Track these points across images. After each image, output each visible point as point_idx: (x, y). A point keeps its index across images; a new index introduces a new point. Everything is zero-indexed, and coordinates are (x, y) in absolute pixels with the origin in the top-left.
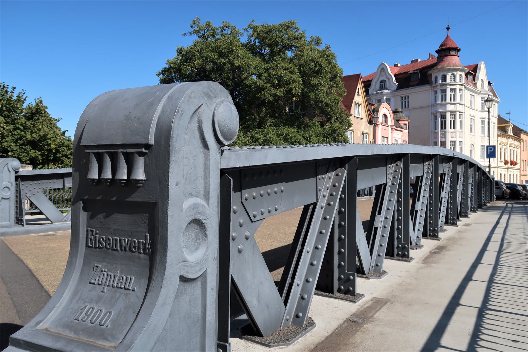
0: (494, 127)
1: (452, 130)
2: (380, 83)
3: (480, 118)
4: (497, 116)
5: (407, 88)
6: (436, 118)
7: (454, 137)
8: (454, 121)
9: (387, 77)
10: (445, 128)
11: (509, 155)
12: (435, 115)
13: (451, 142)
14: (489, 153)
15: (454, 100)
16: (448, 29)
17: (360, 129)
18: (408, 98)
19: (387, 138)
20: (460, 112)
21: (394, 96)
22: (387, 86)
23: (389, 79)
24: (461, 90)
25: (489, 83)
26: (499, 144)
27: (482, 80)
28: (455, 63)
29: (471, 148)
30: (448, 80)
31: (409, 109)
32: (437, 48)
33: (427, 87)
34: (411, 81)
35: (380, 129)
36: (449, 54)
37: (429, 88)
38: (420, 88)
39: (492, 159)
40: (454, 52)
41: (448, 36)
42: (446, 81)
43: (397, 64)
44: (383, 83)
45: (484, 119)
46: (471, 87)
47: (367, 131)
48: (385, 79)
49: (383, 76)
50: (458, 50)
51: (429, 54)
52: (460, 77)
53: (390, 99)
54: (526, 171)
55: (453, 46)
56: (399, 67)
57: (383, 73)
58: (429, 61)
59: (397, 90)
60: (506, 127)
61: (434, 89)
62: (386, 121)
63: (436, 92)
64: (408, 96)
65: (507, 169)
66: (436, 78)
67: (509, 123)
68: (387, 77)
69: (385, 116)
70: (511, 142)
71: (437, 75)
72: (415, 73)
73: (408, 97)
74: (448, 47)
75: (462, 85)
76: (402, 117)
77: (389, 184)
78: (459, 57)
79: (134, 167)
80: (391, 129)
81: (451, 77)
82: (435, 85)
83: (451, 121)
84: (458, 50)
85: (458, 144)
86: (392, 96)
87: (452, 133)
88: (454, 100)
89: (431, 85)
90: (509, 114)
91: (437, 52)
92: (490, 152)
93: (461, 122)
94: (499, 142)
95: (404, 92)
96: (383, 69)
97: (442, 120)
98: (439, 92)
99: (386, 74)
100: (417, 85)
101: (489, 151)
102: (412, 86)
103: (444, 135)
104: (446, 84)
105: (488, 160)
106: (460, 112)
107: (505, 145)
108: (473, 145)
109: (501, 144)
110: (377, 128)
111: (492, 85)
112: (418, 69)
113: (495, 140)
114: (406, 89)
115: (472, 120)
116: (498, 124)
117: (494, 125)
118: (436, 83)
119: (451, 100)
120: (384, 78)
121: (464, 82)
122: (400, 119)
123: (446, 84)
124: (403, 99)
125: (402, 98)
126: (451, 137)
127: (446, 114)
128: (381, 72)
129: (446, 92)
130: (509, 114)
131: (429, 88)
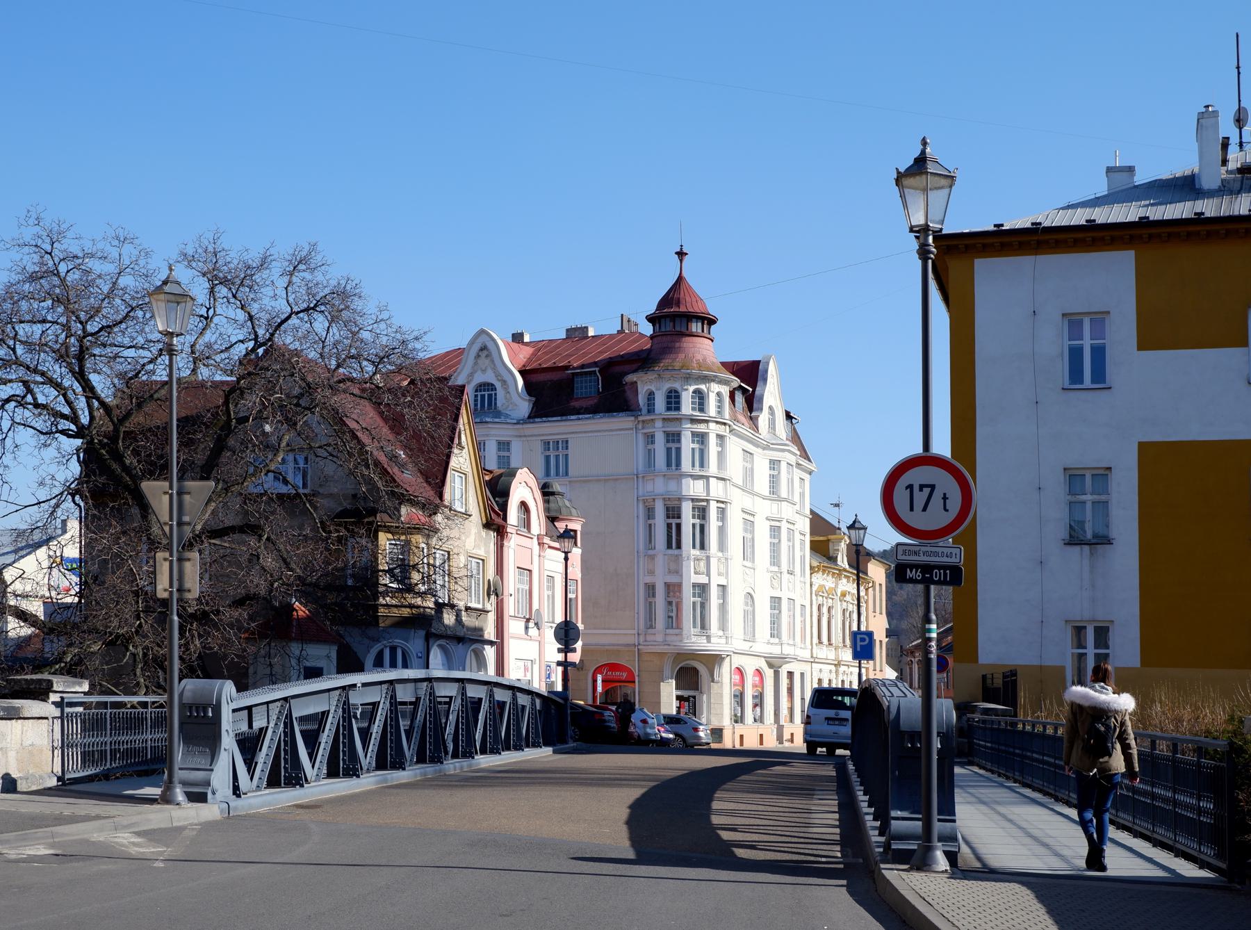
0: (803, 541)
1: (696, 552)
2: (476, 391)
3: (767, 519)
4: (808, 512)
5: (564, 418)
6: (650, 513)
7: (703, 574)
8: (702, 527)
9: (498, 376)
10: (679, 546)
11: (840, 625)
12: (647, 504)
13: (694, 585)
14: (859, 649)
15: (702, 465)
16: (681, 254)
17: (464, 546)
18: (567, 448)
19: (530, 571)
20: (718, 501)
21: (520, 436)
22: (499, 404)
23: (504, 382)
24: (720, 437)
25: (789, 416)
26: (814, 592)
27: (771, 408)
28: (704, 360)
29: (746, 604)
30: (687, 407)
31: (570, 482)
32: (652, 308)
33: (621, 422)
34: (575, 397)
35: (513, 543)
36: (687, 333)
37: (630, 425)
38: (603, 420)
39: (864, 662)
40: (700, 324)
41: (680, 279)
42: (678, 409)
43: (521, 335)
44: (486, 393)
45: (779, 521)
46: (744, 429)
47: (481, 552)
48: (494, 381)
49: (484, 371)
50: (712, 322)
51: (622, 315)
52: (719, 407)
53: (508, 443)
54: (881, 671)
55: (697, 309)
56: (527, 344)
57: (483, 362)
58: (621, 341)
59: (531, 420)
60: (831, 545)
61: (643, 428)
62: (527, 524)
63: (650, 439)
64: (567, 442)
65: (835, 665)
66: (651, 396)
67: (838, 531)
68: (498, 376)
69: (524, 506)
70: (845, 588)
71: (654, 390)
72: (584, 372)
73: (565, 445)
74: (683, 309)
75: (725, 424)
76: (564, 510)
77: (332, 711)
78: (712, 341)
79: (1100, 703)
80: (539, 544)
81: (692, 397)
82: (648, 418)
83: (694, 525)
84: (712, 322)
85: (714, 592)
86: (517, 436)
87: (697, 559)
88: (702, 465)
89: (636, 417)
90: (837, 505)
91: (651, 319)
92: (861, 646)
93: (722, 531)
94: (814, 588)
95: (554, 428)
96: (484, 348)
97: (670, 521)
98: (660, 438)
99: (495, 365)
100: (594, 410)
101: (859, 643)
102: (577, 412)
103: (676, 567)
104: (679, 417)
105: (856, 663)
106: (718, 501)
107: (830, 596)
108: (752, 597)
109: (820, 594)
110: (506, 543)
111: (794, 421)
112: (595, 364)
113: (805, 583)
114: (559, 418)
115: (749, 525)
116: (812, 534)
117: (791, 526)
118: (649, 411)
119: (693, 465)
120: (489, 377)
121: (727, 416)
122: (561, 517)
123: (681, 419)
124: (551, 447)
125: (546, 444)
126: (696, 573)
127: (681, 504)
128: (478, 356)
129: (679, 441)
130: (837, 505)
131: (630, 425)
